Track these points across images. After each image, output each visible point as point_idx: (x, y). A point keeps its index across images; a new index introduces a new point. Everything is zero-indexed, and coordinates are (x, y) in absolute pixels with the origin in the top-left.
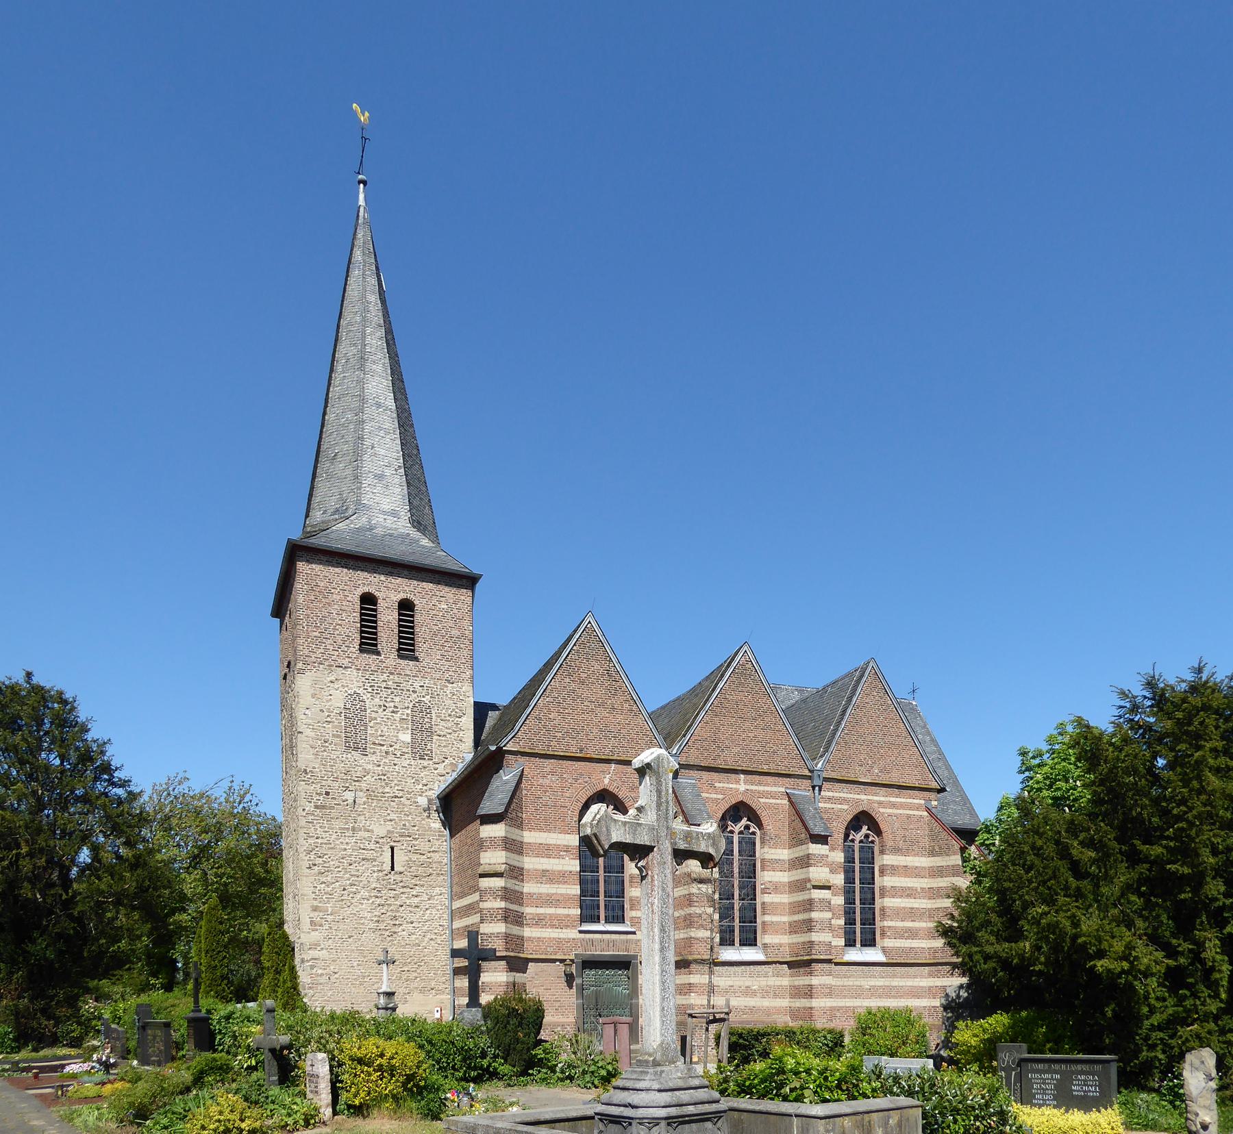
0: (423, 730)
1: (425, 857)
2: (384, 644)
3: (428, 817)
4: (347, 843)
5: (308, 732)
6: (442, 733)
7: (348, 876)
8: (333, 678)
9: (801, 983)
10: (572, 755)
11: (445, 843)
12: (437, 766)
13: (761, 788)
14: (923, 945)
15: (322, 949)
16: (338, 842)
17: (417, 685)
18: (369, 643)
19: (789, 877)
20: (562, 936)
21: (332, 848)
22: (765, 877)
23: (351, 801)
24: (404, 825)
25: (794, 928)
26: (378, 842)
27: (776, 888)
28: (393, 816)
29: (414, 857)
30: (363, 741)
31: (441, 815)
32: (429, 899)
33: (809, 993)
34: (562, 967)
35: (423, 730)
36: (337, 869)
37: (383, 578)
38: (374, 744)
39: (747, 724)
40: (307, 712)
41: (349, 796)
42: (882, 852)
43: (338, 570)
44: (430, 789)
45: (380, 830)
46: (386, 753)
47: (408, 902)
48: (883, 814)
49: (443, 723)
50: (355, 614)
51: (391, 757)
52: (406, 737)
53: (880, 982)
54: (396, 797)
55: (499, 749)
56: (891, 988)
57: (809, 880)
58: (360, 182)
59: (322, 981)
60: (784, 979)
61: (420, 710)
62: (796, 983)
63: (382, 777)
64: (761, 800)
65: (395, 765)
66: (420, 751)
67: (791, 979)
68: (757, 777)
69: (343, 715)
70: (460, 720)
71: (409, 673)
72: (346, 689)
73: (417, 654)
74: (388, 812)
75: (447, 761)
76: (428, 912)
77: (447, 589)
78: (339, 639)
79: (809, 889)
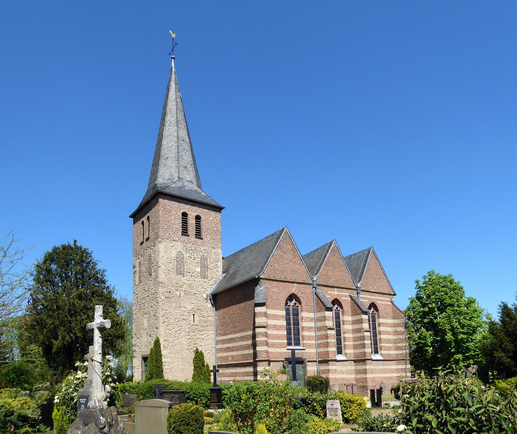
0: (204, 267)
1: (206, 318)
2: (190, 232)
3: (207, 302)
4: (177, 313)
5: (163, 267)
6: (211, 268)
7: (177, 326)
8: (172, 245)
9: (361, 368)
10: (283, 280)
11: (213, 313)
12: (209, 281)
13: (342, 293)
14: (393, 353)
15: (168, 358)
16: (174, 312)
17: (202, 249)
18: (185, 232)
19: (352, 327)
20: (281, 351)
21: (172, 315)
22: (303, 324)
23: (178, 295)
24: (198, 305)
25: (319, 346)
26: (188, 312)
27: (348, 331)
28: (194, 302)
29: (202, 319)
30: (183, 271)
31: (212, 301)
32: (207, 336)
33: (365, 372)
34: (282, 364)
35: (204, 267)
36: (173, 324)
37: (190, 206)
38: (187, 272)
39: (336, 269)
40: (162, 258)
41: (178, 293)
42: (379, 318)
43: (174, 203)
44: (207, 291)
45: (189, 307)
46: (191, 276)
47: (200, 337)
48: (378, 303)
49: (211, 264)
50: (180, 220)
51: (193, 277)
52: (199, 270)
53: (381, 367)
54: (195, 294)
55: (259, 277)
56: (385, 369)
57: (363, 329)
58: (172, 58)
59: (168, 372)
60: (352, 367)
61: (204, 259)
62: (358, 368)
63: (190, 286)
64: (342, 298)
65: (195, 281)
66: (204, 276)
67: (355, 366)
68: (340, 289)
69: (175, 260)
70: (217, 263)
71: (199, 244)
72: (177, 250)
73: (202, 237)
74: (192, 300)
75: (213, 279)
76: (207, 341)
77: (212, 212)
78: (174, 229)
79: (363, 332)
